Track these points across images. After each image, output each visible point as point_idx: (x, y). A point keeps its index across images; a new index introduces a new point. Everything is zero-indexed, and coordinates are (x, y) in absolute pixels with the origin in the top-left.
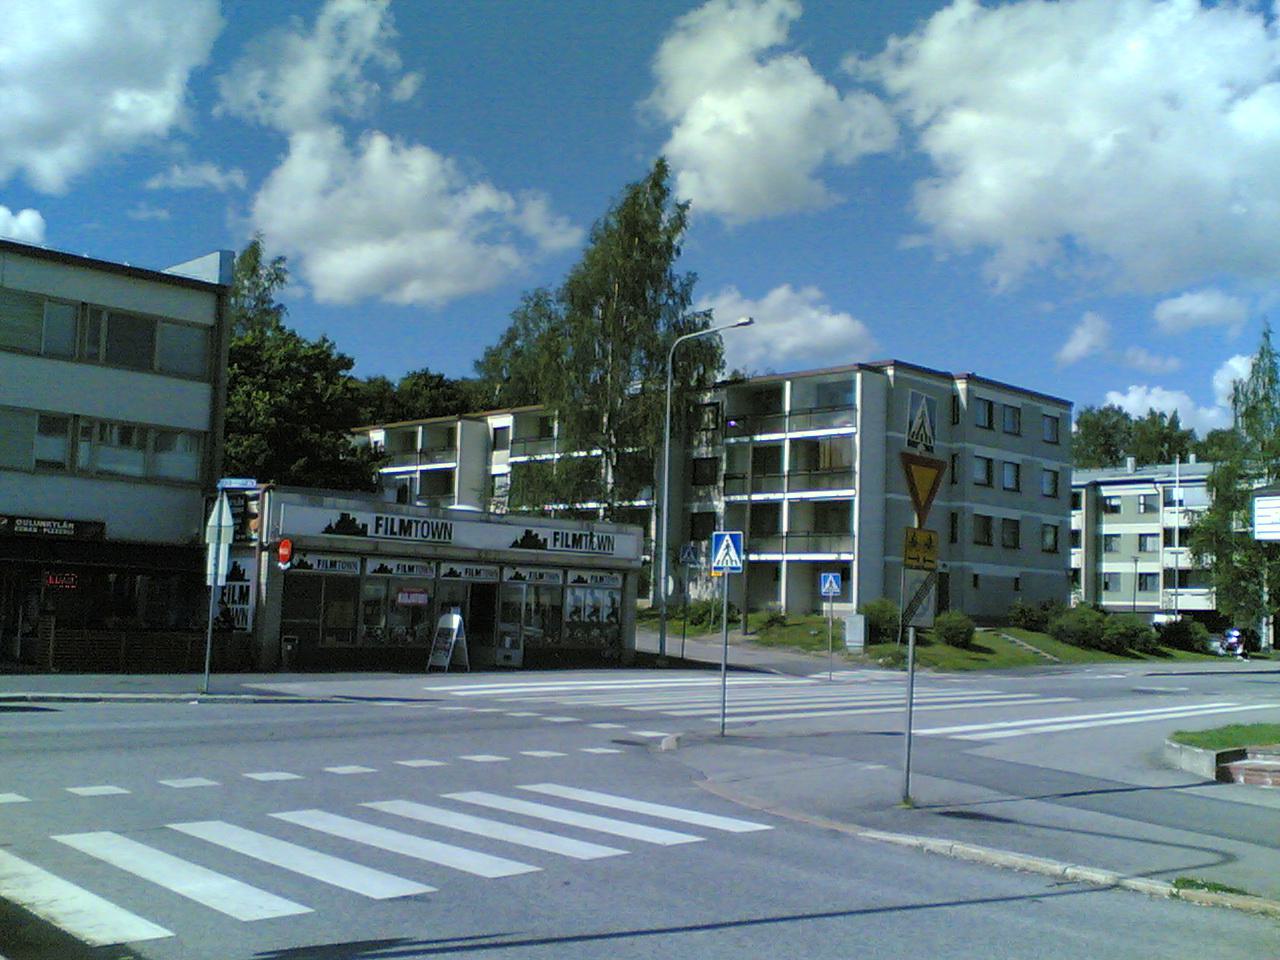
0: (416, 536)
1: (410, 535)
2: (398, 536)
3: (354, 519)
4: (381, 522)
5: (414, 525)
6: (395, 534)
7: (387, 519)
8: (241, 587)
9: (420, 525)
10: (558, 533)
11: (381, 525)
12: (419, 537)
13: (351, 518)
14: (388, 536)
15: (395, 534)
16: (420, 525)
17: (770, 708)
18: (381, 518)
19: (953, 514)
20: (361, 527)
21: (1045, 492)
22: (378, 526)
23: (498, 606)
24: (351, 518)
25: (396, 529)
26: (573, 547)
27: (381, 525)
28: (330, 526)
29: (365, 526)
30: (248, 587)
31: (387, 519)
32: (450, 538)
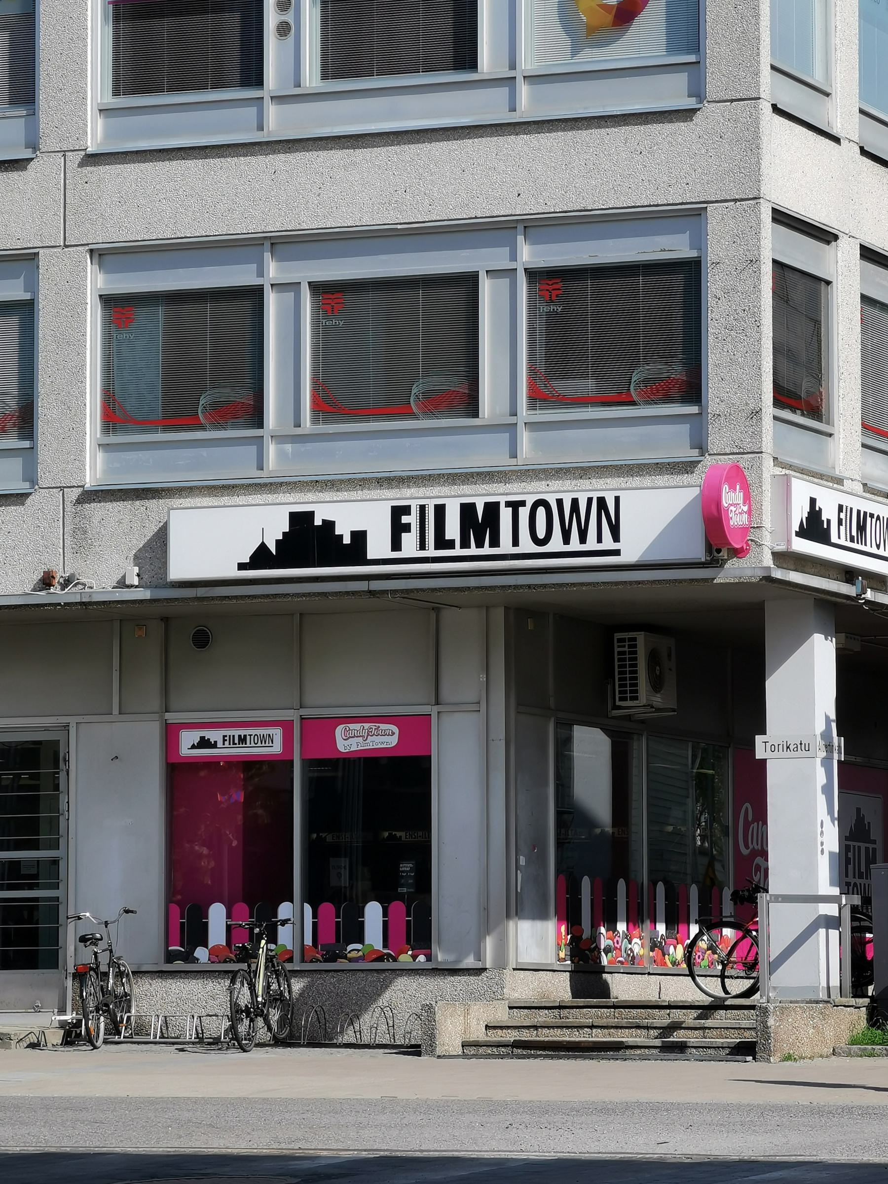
0: (516, 543)
1: (495, 543)
2: (458, 551)
3: (329, 525)
4: (405, 519)
5: (506, 514)
6: (450, 544)
7: (422, 508)
8: (867, 849)
9: (524, 513)
10: (406, 510)
11: (407, 528)
12: (527, 545)
13: (318, 522)
14: (431, 552)
15: (450, 544)
16: (524, 513)
17: (599, 1036)
18: (406, 510)
19: (836, 238)
20: (347, 540)
21: (90, 481)
22: (398, 529)
23: (42, 597)
24: (318, 522)
25: (453, 530)
26: (465, 544)
27: (407, 528)
28: (263, 547)
29: (360, 537)
30: (874, 850)
31: (422, 508)
32: (616, 538)
